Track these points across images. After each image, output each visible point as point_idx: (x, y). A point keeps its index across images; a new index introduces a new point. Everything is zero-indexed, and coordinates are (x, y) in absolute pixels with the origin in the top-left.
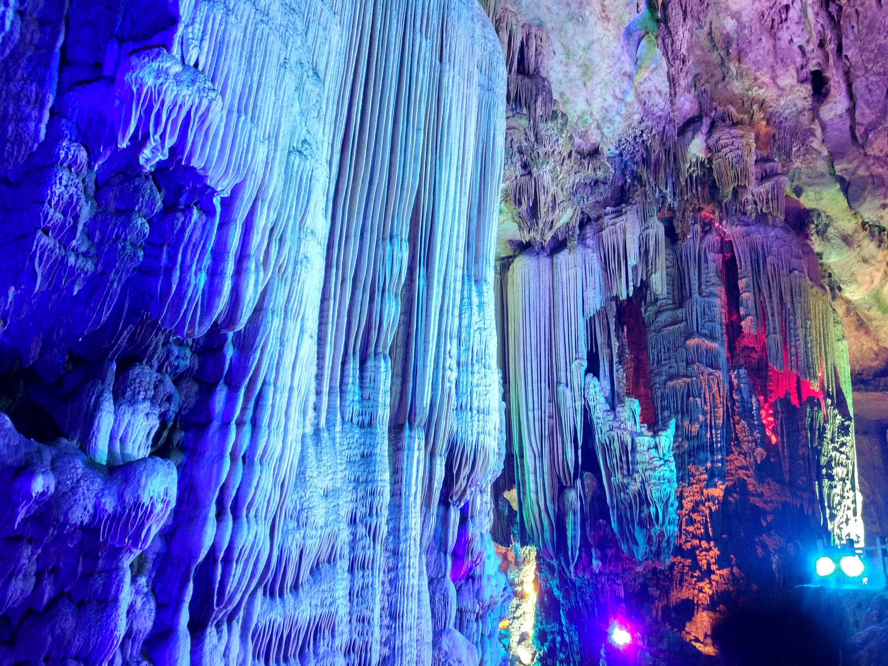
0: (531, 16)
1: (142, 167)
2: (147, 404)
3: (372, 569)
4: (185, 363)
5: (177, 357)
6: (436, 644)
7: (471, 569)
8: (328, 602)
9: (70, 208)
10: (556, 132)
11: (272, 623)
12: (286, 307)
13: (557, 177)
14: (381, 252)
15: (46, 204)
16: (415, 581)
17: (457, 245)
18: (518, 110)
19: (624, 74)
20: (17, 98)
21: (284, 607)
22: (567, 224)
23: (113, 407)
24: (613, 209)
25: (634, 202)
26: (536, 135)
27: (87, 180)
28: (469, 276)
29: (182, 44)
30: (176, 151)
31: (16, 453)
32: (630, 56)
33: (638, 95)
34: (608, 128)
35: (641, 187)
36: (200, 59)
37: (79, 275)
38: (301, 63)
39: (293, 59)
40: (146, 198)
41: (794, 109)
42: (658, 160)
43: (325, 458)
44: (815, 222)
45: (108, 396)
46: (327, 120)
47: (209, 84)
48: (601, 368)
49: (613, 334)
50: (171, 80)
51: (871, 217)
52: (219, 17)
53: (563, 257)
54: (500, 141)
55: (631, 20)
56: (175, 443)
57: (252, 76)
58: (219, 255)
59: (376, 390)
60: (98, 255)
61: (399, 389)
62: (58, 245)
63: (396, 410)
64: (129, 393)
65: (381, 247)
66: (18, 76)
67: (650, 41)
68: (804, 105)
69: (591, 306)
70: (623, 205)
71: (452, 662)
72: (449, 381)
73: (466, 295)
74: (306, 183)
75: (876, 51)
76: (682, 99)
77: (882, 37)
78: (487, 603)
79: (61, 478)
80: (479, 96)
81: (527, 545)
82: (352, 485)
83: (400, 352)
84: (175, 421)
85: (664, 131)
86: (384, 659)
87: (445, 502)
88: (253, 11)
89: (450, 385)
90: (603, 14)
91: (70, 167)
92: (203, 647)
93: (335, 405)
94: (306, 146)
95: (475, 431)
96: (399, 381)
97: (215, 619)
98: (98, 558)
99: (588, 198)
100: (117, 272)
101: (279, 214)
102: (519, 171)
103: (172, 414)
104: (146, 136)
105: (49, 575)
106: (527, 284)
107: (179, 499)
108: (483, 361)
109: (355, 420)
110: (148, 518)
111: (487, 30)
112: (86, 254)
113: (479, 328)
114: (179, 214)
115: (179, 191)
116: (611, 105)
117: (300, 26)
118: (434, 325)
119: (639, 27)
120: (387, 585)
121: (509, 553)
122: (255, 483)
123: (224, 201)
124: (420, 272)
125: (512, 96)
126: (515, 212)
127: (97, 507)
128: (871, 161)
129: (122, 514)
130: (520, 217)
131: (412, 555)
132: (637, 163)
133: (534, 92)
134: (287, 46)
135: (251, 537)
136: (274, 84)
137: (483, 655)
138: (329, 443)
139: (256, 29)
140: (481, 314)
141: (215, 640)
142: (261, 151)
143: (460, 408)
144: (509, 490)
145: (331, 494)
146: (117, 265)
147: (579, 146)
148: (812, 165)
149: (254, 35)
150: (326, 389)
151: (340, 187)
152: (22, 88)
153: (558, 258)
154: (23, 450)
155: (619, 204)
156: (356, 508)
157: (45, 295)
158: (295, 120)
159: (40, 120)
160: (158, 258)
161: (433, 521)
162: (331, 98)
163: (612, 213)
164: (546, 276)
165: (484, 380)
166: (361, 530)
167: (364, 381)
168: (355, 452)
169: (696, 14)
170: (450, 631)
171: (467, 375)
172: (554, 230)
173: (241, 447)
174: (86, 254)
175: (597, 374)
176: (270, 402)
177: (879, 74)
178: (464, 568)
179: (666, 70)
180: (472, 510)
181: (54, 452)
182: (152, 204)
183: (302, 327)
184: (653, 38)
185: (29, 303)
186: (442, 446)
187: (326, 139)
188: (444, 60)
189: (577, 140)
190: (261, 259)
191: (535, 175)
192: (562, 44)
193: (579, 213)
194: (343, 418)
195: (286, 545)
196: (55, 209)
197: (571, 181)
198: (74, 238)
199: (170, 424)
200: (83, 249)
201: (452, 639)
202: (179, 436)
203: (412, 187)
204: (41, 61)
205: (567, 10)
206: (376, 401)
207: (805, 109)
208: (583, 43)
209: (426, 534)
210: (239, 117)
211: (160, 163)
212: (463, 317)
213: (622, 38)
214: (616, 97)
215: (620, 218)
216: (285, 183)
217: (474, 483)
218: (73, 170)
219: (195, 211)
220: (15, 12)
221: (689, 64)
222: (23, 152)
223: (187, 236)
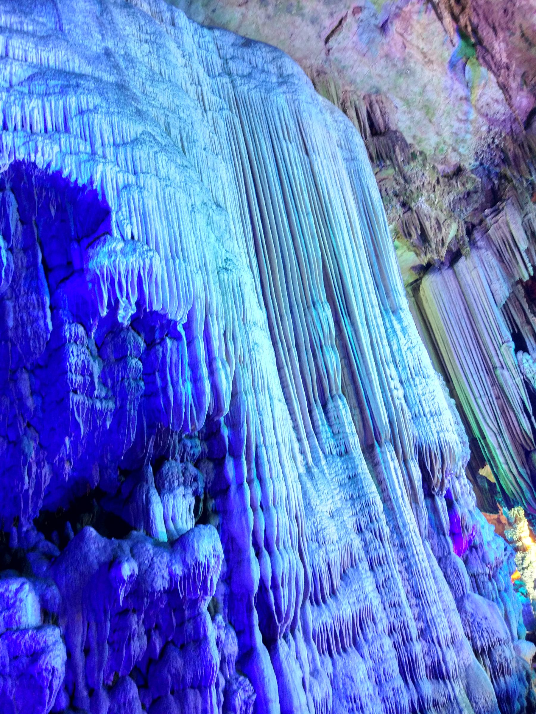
0: (368, 87)
1: (122, 324)
2: (182, 488)
3: (388, 563)
4: (198, 450)
5: (191, 448)
6: (460, 608)
7: (470, 541)
8: (362, 597)
9: (85, 370)
10: (420, 168)
11: (325, 625)
12: (254, 386)
13: (434, 203)
14: (309, 318)
15: (69, 373)
16: (426, 564)
17: (368, 289)
18: (383, 164)
19: (461, 99)
20: (26, 307)
21: (329, 610)
22: (456, 236)
23: (159, 498)
25: (507, 197)
26: (404, 178)
27: (90, 346)
28: (386, 310)
29: (118, 226)
30: (140, 303)
31: (105, 552)
32: (460, 82)
33: (479, 111)
34: (463, 147)
35: (509, 183)
36: (134, 231)
37: (106, 414)
38: (205, 203)
39: (198, 203)
40: (132, 343)
42: (515, 157)
43: (321, 488)
45: (154, 492)
46: (239, 236)
47: (146, 247)
48: (528, 343)
49: (528, 312)
50: (119, 255)
52: (136, 197)
53: (462, 264)
54: (376, 195)
55: (451, 53)
56: (210, 509)
57: (173, 228)
58: (194, 366)
59: (342, 424)
60: (114, 394)
61: (360, 417)
62: (86, 398)
63: (363, 435)
64: (167, 485)
65: (309, 315)
66: (22, 293)
67: (473, 64)
69: (501, 295)
70: (499, 203)
71: (479, 620)
72: (398, 399)
73: (388, 326)
74: (238, 290)
76: (518, 98)
78: (494, 565)
79: (141, 560)
80: (347, 168)
81: (513, 507)
82: (349, 503)
83: (350, 389)
84: (205, 493)
85: (512, 130)
86: (422, 631)
87: (429, 494)
88: (158, 181)
89: (400, 401)
90: (426, 60)
91: (75, 342)
92: (279, 656)
93: (315, 445)
94: (229, 262)
95: (434, 432)
96: (357, 412)
97: (281, 633)
98: (184, 610)
99: (466, 209)
100: (130, 403)
101: (226, 320)
102: (400, 210)
103: (201, 490)
104: (117, 301)
105: (155, 631)
106: (439, 297)
107: (226, 551)
108: (421, 373)
109: (334, 452)
110: (208, 572)
111: (336, 114)
112: (106, 398)
113: (409, 348)
114: (158, 347)
115: (152, 330)
116: (459, 128)
117: (195, 176)
118: (370, 359)
119: (459, 57)
120: (404, 572)
121: (501, 518)
122: (275, 523)
123: (185, 327)
124: (345, 322)
125: (374, 155)
126: (408, 244)
127: (171, 574)
129: (189, 574)
130: (414, 246)
131: (416, 544)
132: (498, 165)
133: (391, 145)
134: (190, 195)
135: (287, 565)
136: (191, 227)
137: (505, 605)
138: (321, 475)
139: (164, 193)
140: (406, 336)
141: (286, 647)
142: (198, 279)
143: (415, 417)
144: (483, 468)
145: (336, 514)
146: (129, 397)
147: (444, 171)
149: (164, 198)
150: (304, 435)
151: (264, 281)
152: (27, 300)
153: (458, 267)
154: (109, 549)
156: (359, 519)
157: (90, 435)
158: (214, 247)
159: (45, 317)
160: (154, 382)
161: (424, 512)
162: (236, 219)
163: (491, 214)
164: (453, 284)
165: (427, 389)
166: (369, 536)
167: (330, 420)
168: (343, 476)
169: (504, 26)
170: (469, 596)
171: (412, 389)
172: (446, 245)
173: (257, 499)
174: (106, 398)
175: (525, 350)
176: (266, 459)
178: (464, 542)
179: (495, 80)
180: (455, 495)
181: (130, 543)
182: (138, 347)
183: (270, 396)
184: (475, 60)
185: (81, 444)
186: (411, 451)
187: (242, 250)
188: (310, 153)
189: (440, 167)
190: (224, 357)
191: (414, 209)
192: (401, 98)
193: (463, 223)
194: (324, 453)
195: (315, 563)
196: (76, 374)
197: (447, 201)
198: (95, 389)
199: (202, 497)
200: (103, 394)
201: (473, 602)
202: (211, 504)
203: (317, 259)
204: (33, 277)
205: (395, 70)
206: (345, 432)
208: (417, 89)
209: (423, 525)
210: (174, 262)
211: (133, 316)
212: (392, 343)
213: (448, 72)
214: (460, 121)
215: (500, 215)
216: (223, 296)
217: (448, 472)
218: (78, 343)
219: (168, 341)
220: (6, 251)
221: (513, 68)
222: (42, 343)
223: (168, 360)
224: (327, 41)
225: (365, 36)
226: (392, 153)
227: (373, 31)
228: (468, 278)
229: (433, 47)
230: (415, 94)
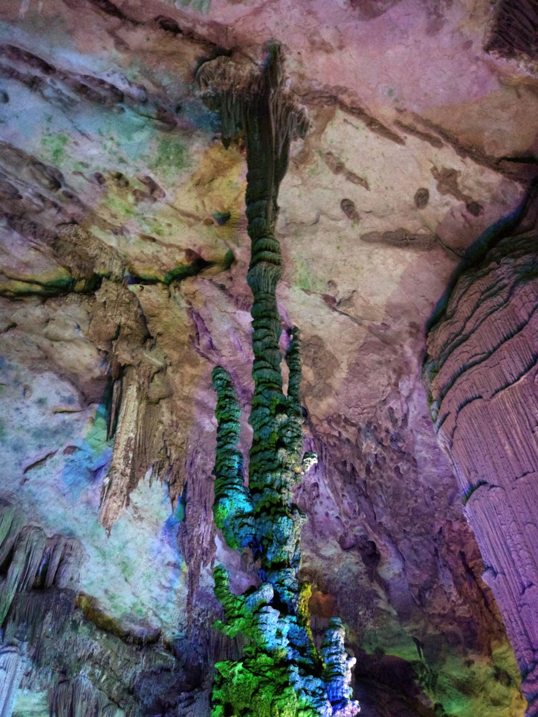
0: (61, 527)
19: (168, 564)
24: (188, 695)
34: (165, 614)
41: (350, 574)
44: (420, 676)
51: (461, 674)
68: (359, 569)
75: (411, 514)
77: (413, 502)
90: (136, 516)
128: (437, 620)
148: (385, 626)
155: (192, 690)
177: (421, 534)
207: (361, 573)
215: (190, 708)
224: (26, 471)
225: (70, 477)
226: (39, 619)
227: (81, 474)
229: (151, 503)
230: (114, 548)
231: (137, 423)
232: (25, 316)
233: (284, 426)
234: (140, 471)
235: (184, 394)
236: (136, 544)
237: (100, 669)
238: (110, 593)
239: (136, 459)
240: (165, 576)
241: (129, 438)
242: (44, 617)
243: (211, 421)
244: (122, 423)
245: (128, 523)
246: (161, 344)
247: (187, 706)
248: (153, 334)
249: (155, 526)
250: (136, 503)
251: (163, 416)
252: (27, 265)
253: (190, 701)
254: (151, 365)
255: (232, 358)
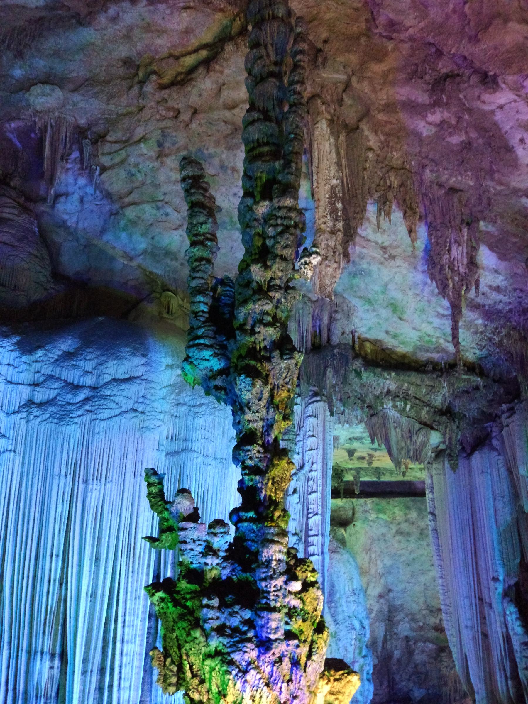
155: (512, 401)
208: (377, 288)
215: (511, 419)
228: (477, 481)
229: (399, 237)
230: (377, 293)
231: (339, 164)
232: (200, 95)
233: (268, 219)
234: (355, 218)
235: (383, 102)
236: (396, 284)
237: (401, 400)
238: (392, 333)
239: (347, 206)
240: (440, 305)
241: (332, 187)
242: (325, 374)
243: (426, 122)
244: (317, 174)
245: (380, 266)
246: (331, 53)
247: (509, 417)
248: (319, 45)
249: (412, 260)
250: (383, 243)
251: (369, 141)
252: (188, 31)
253: (512, 412)
254: (336, 83)
255: (422, 24)
